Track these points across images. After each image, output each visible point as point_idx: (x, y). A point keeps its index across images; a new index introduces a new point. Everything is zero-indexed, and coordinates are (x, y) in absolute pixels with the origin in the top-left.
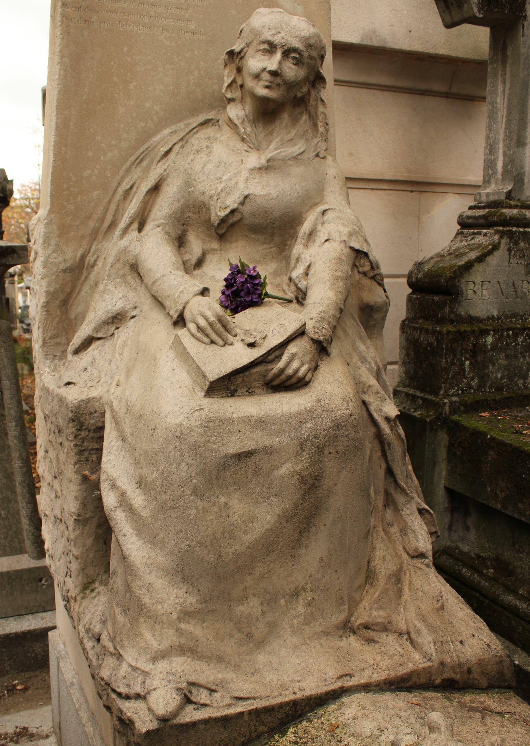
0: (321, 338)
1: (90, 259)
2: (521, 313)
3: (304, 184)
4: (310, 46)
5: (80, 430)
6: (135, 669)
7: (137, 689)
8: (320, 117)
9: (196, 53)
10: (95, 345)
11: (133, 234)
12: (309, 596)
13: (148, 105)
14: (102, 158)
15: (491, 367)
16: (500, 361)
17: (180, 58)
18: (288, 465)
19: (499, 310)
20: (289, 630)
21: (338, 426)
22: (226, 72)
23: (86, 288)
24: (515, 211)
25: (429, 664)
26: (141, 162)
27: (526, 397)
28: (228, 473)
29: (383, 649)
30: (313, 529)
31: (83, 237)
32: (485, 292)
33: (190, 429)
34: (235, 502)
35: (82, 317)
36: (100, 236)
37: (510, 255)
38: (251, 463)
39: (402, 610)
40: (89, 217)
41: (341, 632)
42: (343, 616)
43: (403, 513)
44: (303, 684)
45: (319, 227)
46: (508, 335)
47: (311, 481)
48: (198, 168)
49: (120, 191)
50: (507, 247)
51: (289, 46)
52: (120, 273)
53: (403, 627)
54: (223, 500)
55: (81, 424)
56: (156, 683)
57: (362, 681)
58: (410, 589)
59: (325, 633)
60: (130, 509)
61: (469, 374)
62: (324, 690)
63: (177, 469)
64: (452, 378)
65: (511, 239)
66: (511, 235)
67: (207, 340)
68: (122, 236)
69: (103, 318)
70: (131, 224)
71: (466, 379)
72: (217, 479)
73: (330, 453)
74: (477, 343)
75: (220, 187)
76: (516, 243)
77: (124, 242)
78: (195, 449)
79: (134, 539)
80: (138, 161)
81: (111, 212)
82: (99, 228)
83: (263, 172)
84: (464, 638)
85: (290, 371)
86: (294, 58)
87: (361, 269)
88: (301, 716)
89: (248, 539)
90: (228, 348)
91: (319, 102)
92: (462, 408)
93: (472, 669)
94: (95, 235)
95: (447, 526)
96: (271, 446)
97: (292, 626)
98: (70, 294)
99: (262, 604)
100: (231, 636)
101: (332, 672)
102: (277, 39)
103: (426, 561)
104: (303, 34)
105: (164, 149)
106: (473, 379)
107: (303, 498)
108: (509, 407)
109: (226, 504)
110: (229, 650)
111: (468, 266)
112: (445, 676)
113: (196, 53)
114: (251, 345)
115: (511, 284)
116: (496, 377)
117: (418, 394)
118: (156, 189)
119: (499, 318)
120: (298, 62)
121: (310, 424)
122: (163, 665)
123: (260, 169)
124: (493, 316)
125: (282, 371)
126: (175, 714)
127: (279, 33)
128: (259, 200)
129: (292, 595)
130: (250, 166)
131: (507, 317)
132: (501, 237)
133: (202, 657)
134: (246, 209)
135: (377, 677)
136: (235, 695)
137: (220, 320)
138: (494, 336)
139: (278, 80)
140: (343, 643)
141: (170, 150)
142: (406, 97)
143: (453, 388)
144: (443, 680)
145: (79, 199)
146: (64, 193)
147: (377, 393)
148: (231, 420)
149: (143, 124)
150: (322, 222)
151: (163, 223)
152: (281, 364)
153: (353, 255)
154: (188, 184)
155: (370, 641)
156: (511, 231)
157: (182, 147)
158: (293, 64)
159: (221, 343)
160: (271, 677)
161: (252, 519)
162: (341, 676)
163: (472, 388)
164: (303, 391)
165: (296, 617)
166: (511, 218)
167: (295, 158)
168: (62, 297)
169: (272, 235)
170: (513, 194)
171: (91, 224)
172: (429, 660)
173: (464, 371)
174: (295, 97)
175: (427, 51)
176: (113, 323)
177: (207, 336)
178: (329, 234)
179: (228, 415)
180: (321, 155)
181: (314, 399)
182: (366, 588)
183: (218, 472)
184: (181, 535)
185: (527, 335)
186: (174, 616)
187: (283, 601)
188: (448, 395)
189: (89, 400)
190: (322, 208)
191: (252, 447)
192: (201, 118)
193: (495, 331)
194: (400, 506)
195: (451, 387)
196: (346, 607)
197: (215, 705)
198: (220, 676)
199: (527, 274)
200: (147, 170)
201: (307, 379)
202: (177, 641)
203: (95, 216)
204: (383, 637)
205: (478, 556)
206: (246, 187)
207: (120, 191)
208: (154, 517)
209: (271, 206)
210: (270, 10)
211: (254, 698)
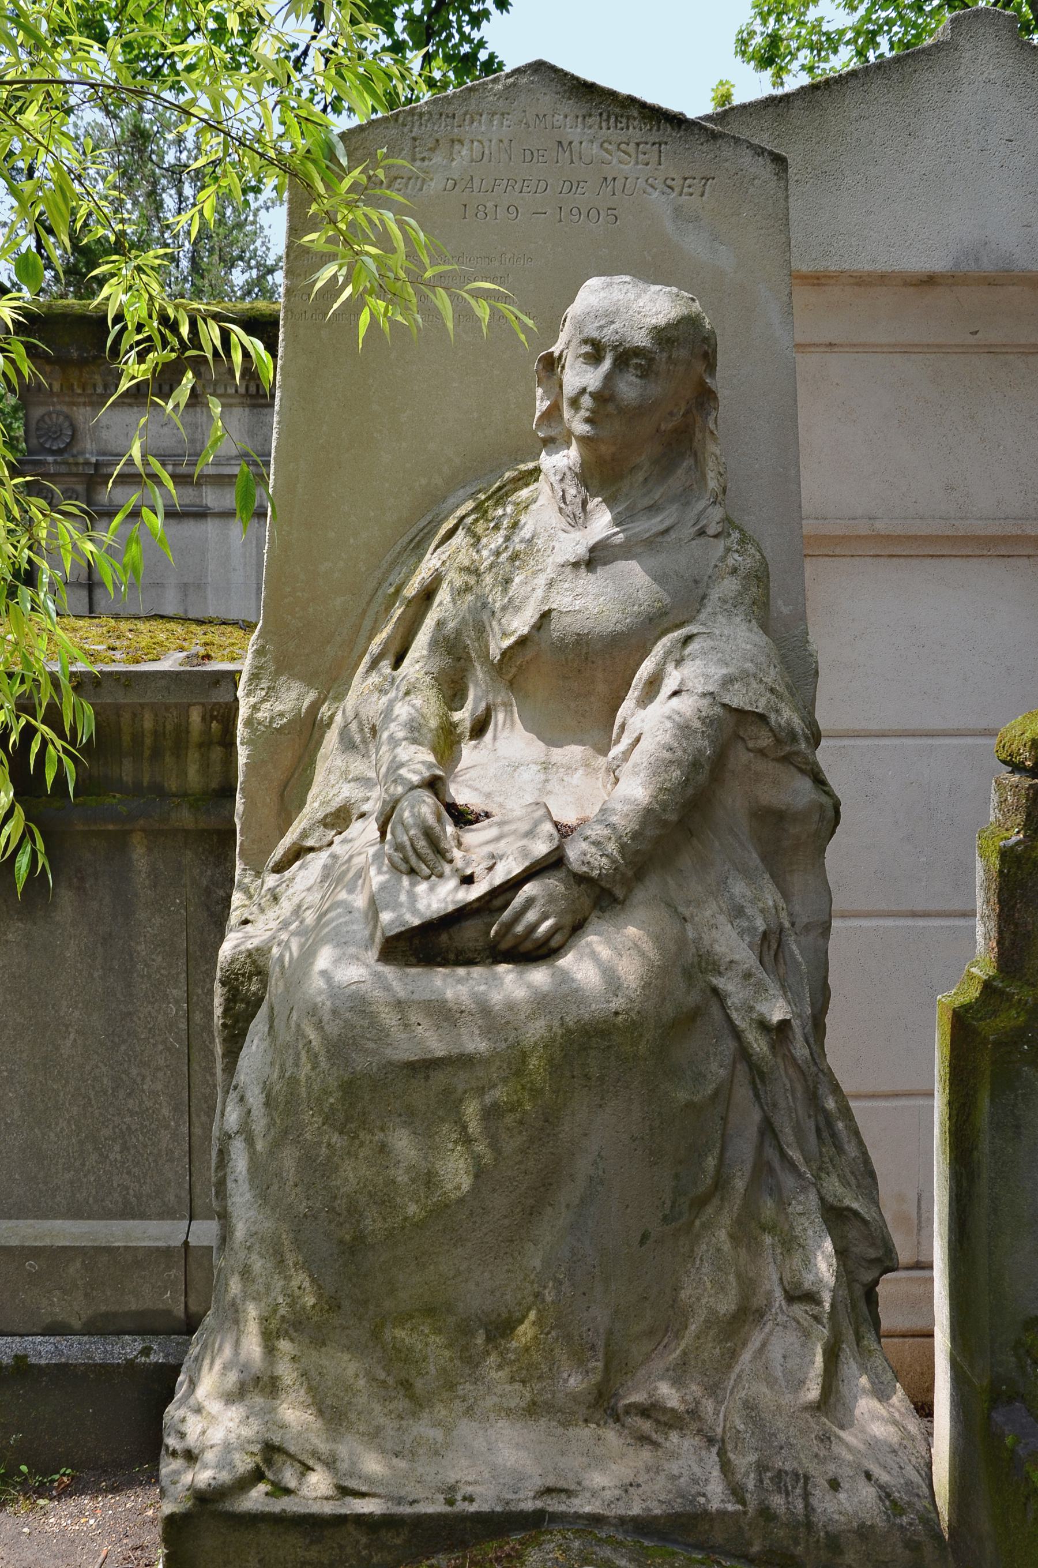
14: (352, 541)
17: (491, 363)
43: (790, 1210)
51: (627, 345)
73: (573, 1077)
80: (412, 545)
86: (638, 366)
91: (707, 434)
102: (608, 335)
103: (815, 1310)
120: (645, 373)
123: (576, 565)
127: (613, 322)
128: (567, 620)
145: (311, 610)
146: (286, 601)
149: (424, 481)
150: (678, 657)
151: (424, 657)
155: (644, 1439)
158: (637, 376)
159: (427, 871)
177: (406, 860)
180: (712, 530)
182: (666, 1340)
196: (600, 1365)
207: (379, 598)
209: (586, 632)
210: (608, 279)
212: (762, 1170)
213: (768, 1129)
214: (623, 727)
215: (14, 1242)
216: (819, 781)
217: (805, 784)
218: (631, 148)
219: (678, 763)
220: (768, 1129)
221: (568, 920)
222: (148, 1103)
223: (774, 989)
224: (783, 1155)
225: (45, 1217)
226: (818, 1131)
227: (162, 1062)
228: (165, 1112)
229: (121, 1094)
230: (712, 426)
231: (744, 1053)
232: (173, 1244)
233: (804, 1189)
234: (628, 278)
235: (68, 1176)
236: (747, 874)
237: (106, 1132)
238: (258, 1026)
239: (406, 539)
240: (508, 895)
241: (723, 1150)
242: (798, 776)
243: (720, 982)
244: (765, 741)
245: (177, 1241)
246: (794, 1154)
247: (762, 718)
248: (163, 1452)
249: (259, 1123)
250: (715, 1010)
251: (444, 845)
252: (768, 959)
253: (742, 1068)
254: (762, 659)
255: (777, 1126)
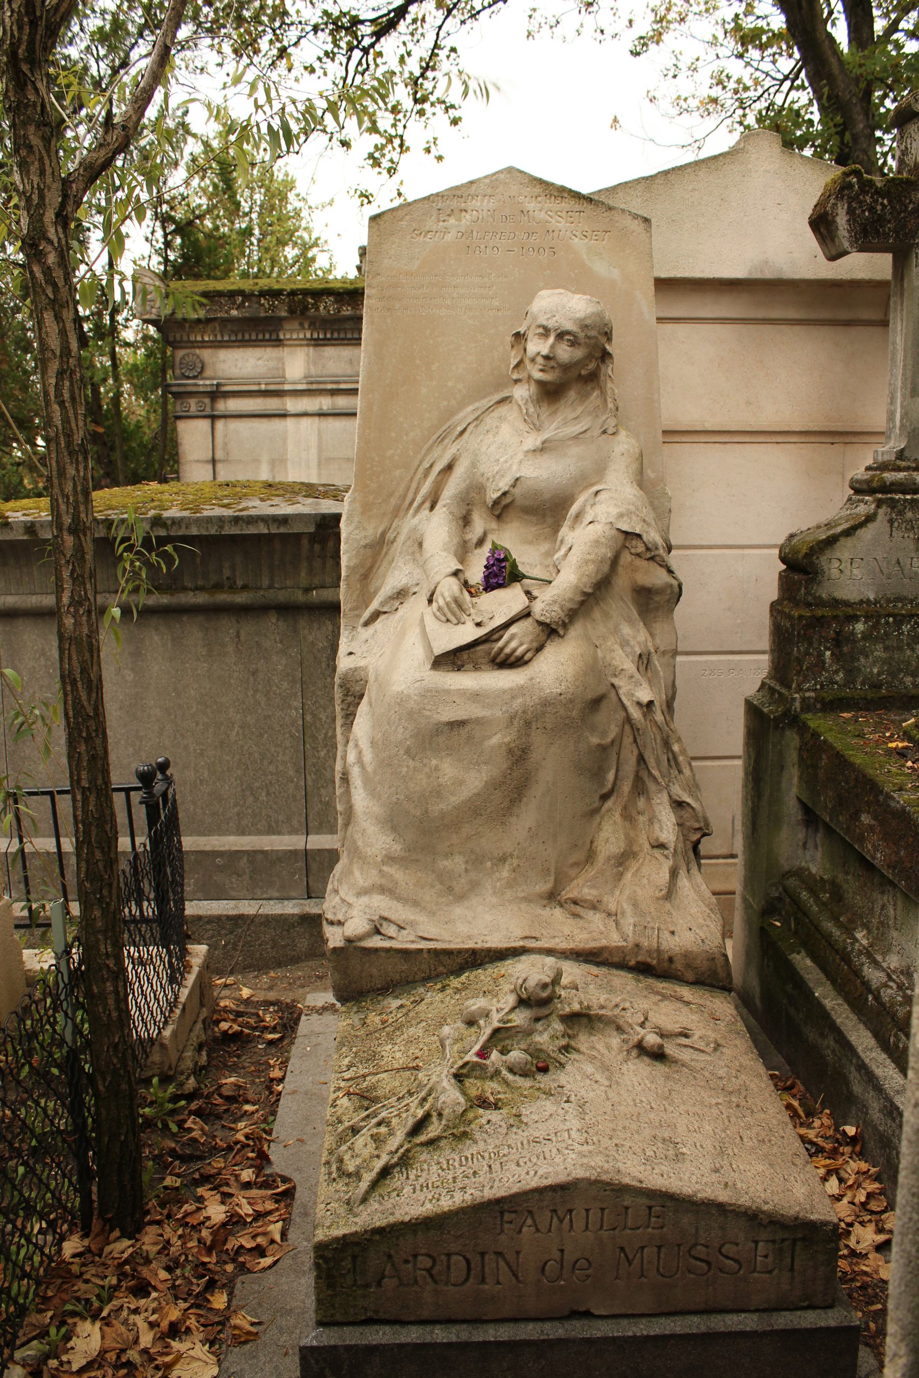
0: (548, 621)
1: (390, 535)
2: (910, 597)
3: (579, 464)
4: (586, 326)
5: (346, 695)
6: (343, 901)
7: (340, 917)
8: (609, 392)
9: (501, 328)
10: (382, 618)
11: (425, 512)
12: (515, 862)
13: (450, 384)
15: (862, 660)
16: (876, 653)
18: (499, 736)
19: (876, 593)
20: (491, 891)
21: (546, 703)
22: (513, 353)
23: (385, 563)
24: (901, 475)
25: (624, 944)
26: (443, 440)
27: (913, 697)
28: (441, 739)
29: (586, 925)
30: (525, 799)
31: (384, 514)
32: (855, 571)
33: (409, 696)
34: (446, 765)
35: (376, 592)
36: (402, 514)
37: (891, 526)
38: (464, 731)
39: (618, 893)
40: (391, 495)
41: (545, 902)
42: (548, 886)
44: (488, 938)
45: (588, 508)
46: (887, 623)
47: (518, 753)
48: (484, 449)
49: (421, 470)
50: (888, 517)
52: (410, 551)
53: (612, 907)
54: (434, 762)
55: (348, 690)
56: (355, 912)
57: (546, 946)
58: (634, 875)
59: (527, 900)
60: (363, 766)
61: (830, 666)
62: (505, 945)
63: (395, 731)
64: (807, 668)
65: (893, 508)
66: (892, 504)
67: (444, 619)
68: (414, 515)
69: (389, 594)
70: (423, 503)
71: (827, 671)
72: (430, 743)
74: (841, 631)
75: (497, 468)
76: (901, 513)
77: (415, 521)
78: (411, 714)
79: (361, 791)
81: (412, 490)
82: (401, 505)
83: (538, 454)
84: (677, 929)
85: (507, 650)
86: (569, 340)
87: (633, 551)
88: (480, 965)
89: (455, 800)
90: (461, 626)
92: (819, 706)
93: (675, 959)
94: (397, 513)
95: (801, 843)
96: (483, 718)
97: (494, 887)
98: (371, 568)
99: (467, 862)
100: (433, 886)
101: (519, 933)
102: (551, 324)
103: (666, 852)
104: (578, 316)
105: (460, 429)
106: (836, 672)
107: (511, 769)
108: (886, 708)
109: (436, 766)
110: (428, 898)
111: (831, 541)
112: (640, 958)
113: (501, 328)
114: (478, 625)
115: (894, 562)
116: (871, 672)
117: (778, 688)
118: (449, 468)
119: (876, 602)
120: (574, 343)
121: (520, 700)
122: (364, 900)
123: (534, 451)
124: (868, 600)
125: (502, 649)
126: (361, 938)
129: (500, 860)
130: (525, 448)
131: (889, 601)
132: (878, 507)
133: (399, 899)
134: (517, 491)
135: (564, 945)
136: (421, 934)
137: (456, 601)
138: (865, 622)
139: (552, 363)
140: (546, 912)
141: (465, 430)
142: (824, 331)
143: (809, 681)
144: (638, 962)
147: (632, 677)
148: (448, 692)
149: (445, 403)
152: (500, 644)
153: (621, 537)
154: (474, 465)
155: (576, 916)
156: (892, 499)
157: (477, 426)
159: (455, 621)
160: (463, 928)
161: (461, 783)
162: (526, 937)
163: (836, 683)
164: (520, 670)
165: (499, 880)
166: (892, 484)
167: (576, 438)
168: (362, 571)
169: (544, 516)
170: (906, 454)
171: (393, 501)
172: (625, 940)
173: (824, 662)
174: (580, 375)
175: (840, 277)
176: (398, 598)
177: (445, 615)
178: (595, 516)
179: (446, 687)
180: (610, 431)
181: (528, 676)
183: (432, 737)
184: (393, 789)
185: (916, 623)
186: (379, 859)
187: (489, 864)
188: (801, 690)
189: (356, 669)
190: (596, 488)
191: (465, 718)
192: (497, 397)
193: (868, 618)
194: (652, 795)
195: (806, 680)
197: (400, 938)
198: (412, 918)
199: (917, 550)
200: (444, 450)
201: (526, 658)
202: (379, 881)
203: (397, 494)
204: (589, 914)
205: (821, 878)
206: (519, 470)
207: (421, 470)
208: (375, 772)
211: (437, 940)
212: (638, 779)
213: (641, 759)
214: (562, 541)
215: (208, 848)
216: (670, 572)
217: (663, 573)
218: (564, 214)
219: (593, 562)
220: (641, 759)
221: (535, 645)
222: (281, 768)
223: (645, 685)
224: (650, 774)
225: (225, 835)
226: (668, 760)
227: (288, 744)
228: (291, 773)
229: (265, 763)
230: (610, 373)
231: (628, 719)
232: (298, 848)
233: (660, 791)
234: (562, 291)
235: (236, 810)
236: (630, 622)
237: (257, 784)
238: (363, 707)
239: (436, 436)
240: (501, 633)
241: (617, 770)
242: (659, 568)
243: (616, 681)
244: (641, 548)
245: (310, 837)
246: (655, 773)
247: (639, 536)
248: (324, 922)
249: (368, 757)
250: (613, 695)
251: (465, 607)
252: (642, 668)
253: (627, 728)
254: (639, 503)
255: (646, 757)
